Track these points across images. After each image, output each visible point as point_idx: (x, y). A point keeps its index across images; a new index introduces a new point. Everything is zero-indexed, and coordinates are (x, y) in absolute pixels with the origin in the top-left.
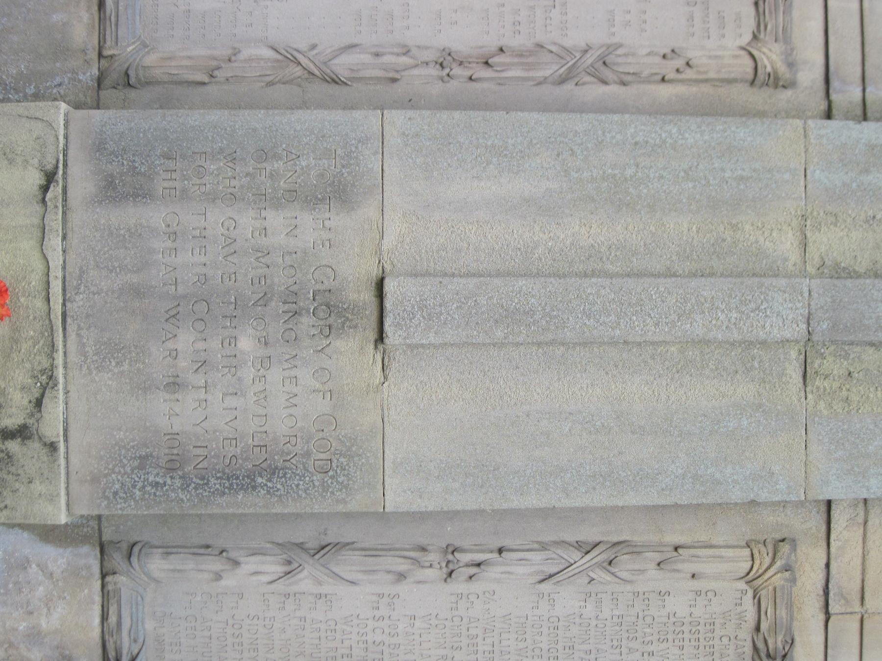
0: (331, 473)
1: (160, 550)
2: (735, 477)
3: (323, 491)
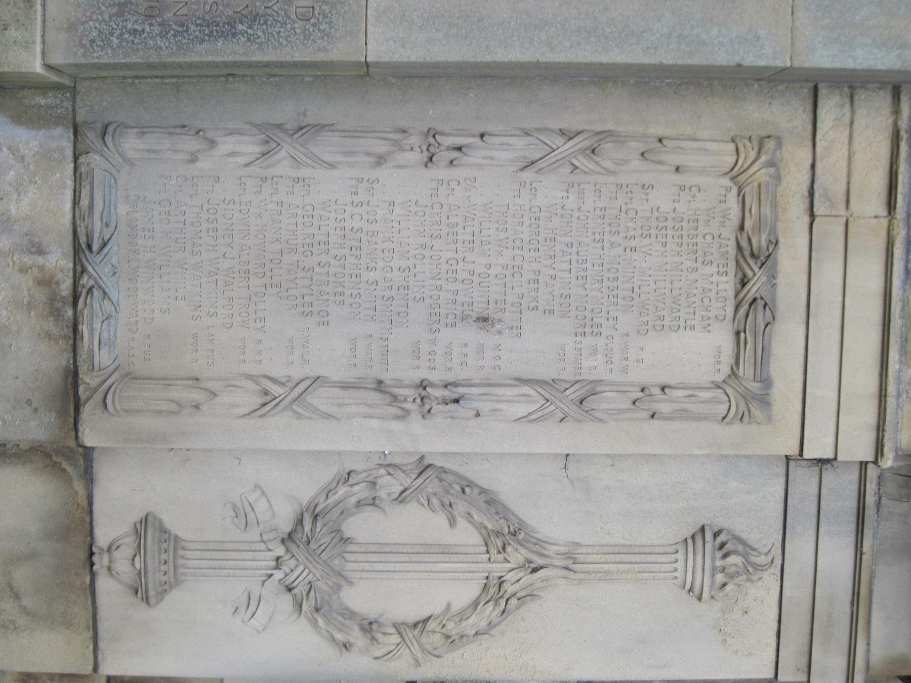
0: (313, 21)
1: (135, 130)
2: (721, 39)
3: (305, 39)
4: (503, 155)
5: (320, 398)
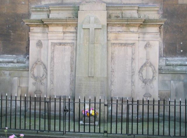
4: (113, 66)
5: (133, 80)
